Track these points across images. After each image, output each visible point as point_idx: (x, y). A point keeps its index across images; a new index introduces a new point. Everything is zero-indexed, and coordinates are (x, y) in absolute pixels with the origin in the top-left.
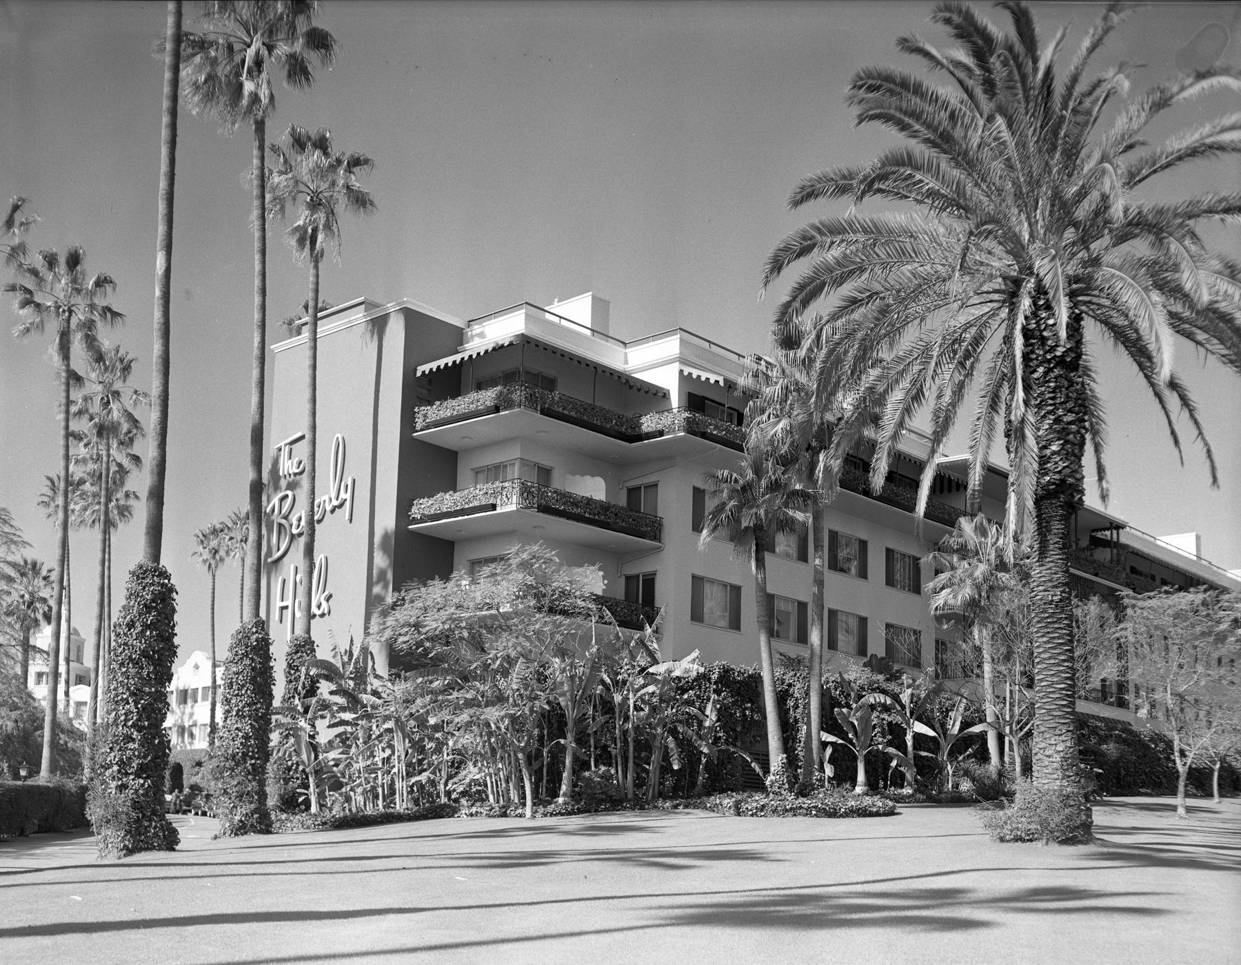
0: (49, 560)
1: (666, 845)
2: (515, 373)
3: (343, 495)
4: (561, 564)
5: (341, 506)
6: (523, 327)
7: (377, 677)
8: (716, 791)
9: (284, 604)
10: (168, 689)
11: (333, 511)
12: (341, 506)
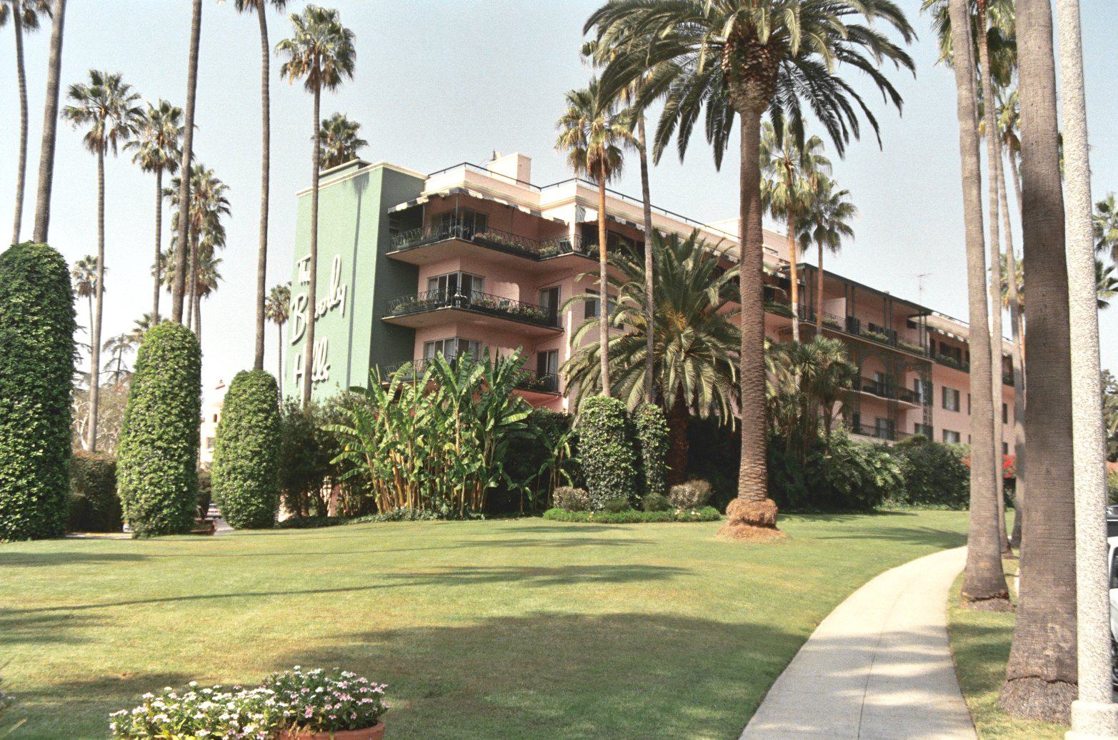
0: (180, 102)
1: (291, 537)
2: (448, 215)
3: (338, 298)
4: (522, 310)
5: (337, 305)
6: (251, 369)
7: (681, 346)
8: (271, 512)
9: (299, 372)
10: (260, 438)
11: (332, 309)
12: (337, 305)
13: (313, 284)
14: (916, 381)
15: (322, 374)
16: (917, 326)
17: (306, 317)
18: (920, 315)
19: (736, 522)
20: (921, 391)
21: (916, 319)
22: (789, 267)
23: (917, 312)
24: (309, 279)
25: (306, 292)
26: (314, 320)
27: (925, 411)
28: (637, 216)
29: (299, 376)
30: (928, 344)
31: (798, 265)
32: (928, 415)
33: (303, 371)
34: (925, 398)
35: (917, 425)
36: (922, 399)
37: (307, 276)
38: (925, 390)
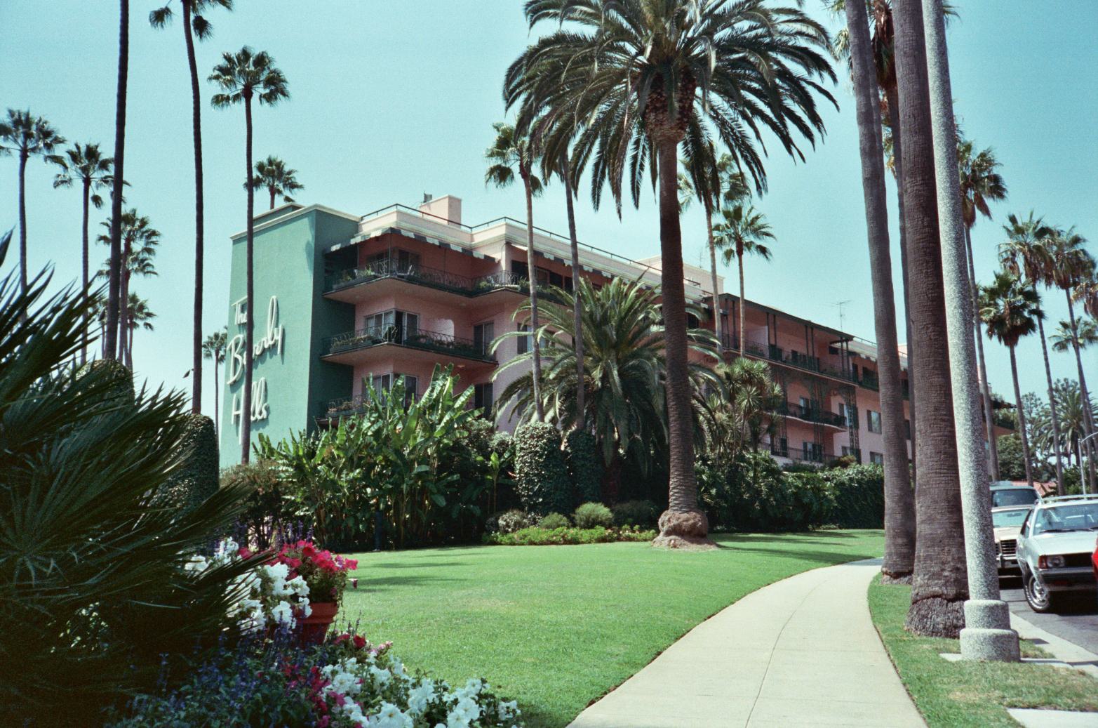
3: (276, 338)
13: (249, 326)
14: (841, 406)
15: (261, 413)
16: (840, 351)
17: (243, 360)
18: (842, 341)
19: (668, 533)
20: (846, 414)
21: (838, 345)
22: (711, 298)
23: (839, 339)
24: (245, 320)
25: (242, 336)
26: (251, 363)
27: (851, 434)
28: (566, 254)
29: (237, 417)
30: (851, 368)
31: (721, 296)
32: (854, 438)
33: (241, 412)
34: (851, 421)
35: (844, 448)
36: (848, 423)
37: (243, 318)
38: (850, 414)
